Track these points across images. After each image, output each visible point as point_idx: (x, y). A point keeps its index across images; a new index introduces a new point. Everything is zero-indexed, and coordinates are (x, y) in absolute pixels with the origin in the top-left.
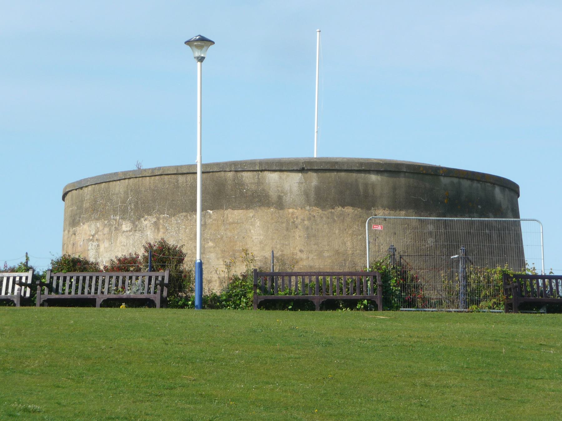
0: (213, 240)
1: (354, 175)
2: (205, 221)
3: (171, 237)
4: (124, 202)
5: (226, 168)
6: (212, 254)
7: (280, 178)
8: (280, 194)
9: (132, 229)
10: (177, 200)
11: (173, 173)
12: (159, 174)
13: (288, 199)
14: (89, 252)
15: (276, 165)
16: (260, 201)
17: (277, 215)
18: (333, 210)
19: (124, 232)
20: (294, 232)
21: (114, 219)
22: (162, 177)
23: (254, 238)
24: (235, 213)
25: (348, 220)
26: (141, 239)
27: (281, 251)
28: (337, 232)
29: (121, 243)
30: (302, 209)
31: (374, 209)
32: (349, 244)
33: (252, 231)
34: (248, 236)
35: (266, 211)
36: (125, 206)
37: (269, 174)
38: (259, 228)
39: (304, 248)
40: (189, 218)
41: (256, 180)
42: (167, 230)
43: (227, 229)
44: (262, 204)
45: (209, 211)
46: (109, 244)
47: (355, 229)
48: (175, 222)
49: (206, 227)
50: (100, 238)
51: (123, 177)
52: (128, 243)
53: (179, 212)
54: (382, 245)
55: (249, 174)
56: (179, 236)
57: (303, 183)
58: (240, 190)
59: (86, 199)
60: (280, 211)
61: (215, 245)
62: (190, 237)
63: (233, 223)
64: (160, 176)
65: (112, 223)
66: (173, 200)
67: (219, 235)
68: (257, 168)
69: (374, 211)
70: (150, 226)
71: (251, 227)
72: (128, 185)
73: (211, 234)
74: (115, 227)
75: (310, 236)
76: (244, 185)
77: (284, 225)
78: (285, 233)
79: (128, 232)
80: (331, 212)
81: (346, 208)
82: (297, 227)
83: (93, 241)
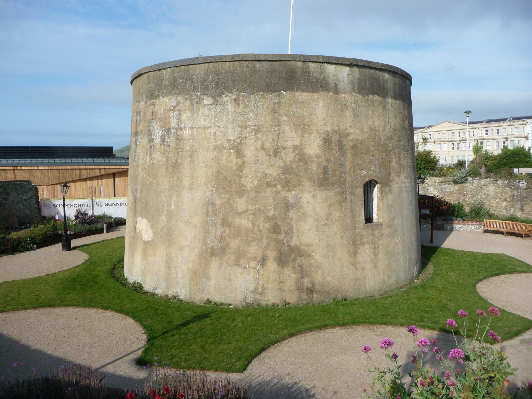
0: (287, 116)
1: (378, 72)
2: (280, 100)
3: (251, 111)
4: (204, 81)
6: (287, 127)
7: (336, 69)
9: (213, 103)
10: (255, 82)
11: (252, 59)
12: (238, 60)
13: (341, 86)
14: (171, 119)
15: (334, 59)
16: (322, 86)
17: (335, 98)
18: (368, 97)
19: (205, 105)
20: (346, 112)
21: (195, 95)
22: (241, 62)
23: (319, 115)
24: (304, 95)
27: (338, 126)
29: (203, 114)
30: (350, 94)
33: (317, 110)
34: (314, 113)
35: (327, 94)
36: (206, 85)
37: (328, 66)
40: (266, 96)
43: (298, 107)
44: (324, 89)
45: (283, 92)
48: (254, 99)
49: (280, 105)
50: (182, 109)
51: (204, 62)
52: (210, 114)
53: (257, 91)
55: (314, 64)
59: (165, 78)
60: (336, 95)
61: (288, 120)
64: (238, 62)
65: (193, 98)
66: (251, 82)
67: (292, 111)
68: (321, 60)
70: (231, 102)
71: (316, 107)
73: (285, 111)
74: (197, 101)
75: (356, 116)
77: (339, 106)
81: (375, 96)
83: (175, 111)
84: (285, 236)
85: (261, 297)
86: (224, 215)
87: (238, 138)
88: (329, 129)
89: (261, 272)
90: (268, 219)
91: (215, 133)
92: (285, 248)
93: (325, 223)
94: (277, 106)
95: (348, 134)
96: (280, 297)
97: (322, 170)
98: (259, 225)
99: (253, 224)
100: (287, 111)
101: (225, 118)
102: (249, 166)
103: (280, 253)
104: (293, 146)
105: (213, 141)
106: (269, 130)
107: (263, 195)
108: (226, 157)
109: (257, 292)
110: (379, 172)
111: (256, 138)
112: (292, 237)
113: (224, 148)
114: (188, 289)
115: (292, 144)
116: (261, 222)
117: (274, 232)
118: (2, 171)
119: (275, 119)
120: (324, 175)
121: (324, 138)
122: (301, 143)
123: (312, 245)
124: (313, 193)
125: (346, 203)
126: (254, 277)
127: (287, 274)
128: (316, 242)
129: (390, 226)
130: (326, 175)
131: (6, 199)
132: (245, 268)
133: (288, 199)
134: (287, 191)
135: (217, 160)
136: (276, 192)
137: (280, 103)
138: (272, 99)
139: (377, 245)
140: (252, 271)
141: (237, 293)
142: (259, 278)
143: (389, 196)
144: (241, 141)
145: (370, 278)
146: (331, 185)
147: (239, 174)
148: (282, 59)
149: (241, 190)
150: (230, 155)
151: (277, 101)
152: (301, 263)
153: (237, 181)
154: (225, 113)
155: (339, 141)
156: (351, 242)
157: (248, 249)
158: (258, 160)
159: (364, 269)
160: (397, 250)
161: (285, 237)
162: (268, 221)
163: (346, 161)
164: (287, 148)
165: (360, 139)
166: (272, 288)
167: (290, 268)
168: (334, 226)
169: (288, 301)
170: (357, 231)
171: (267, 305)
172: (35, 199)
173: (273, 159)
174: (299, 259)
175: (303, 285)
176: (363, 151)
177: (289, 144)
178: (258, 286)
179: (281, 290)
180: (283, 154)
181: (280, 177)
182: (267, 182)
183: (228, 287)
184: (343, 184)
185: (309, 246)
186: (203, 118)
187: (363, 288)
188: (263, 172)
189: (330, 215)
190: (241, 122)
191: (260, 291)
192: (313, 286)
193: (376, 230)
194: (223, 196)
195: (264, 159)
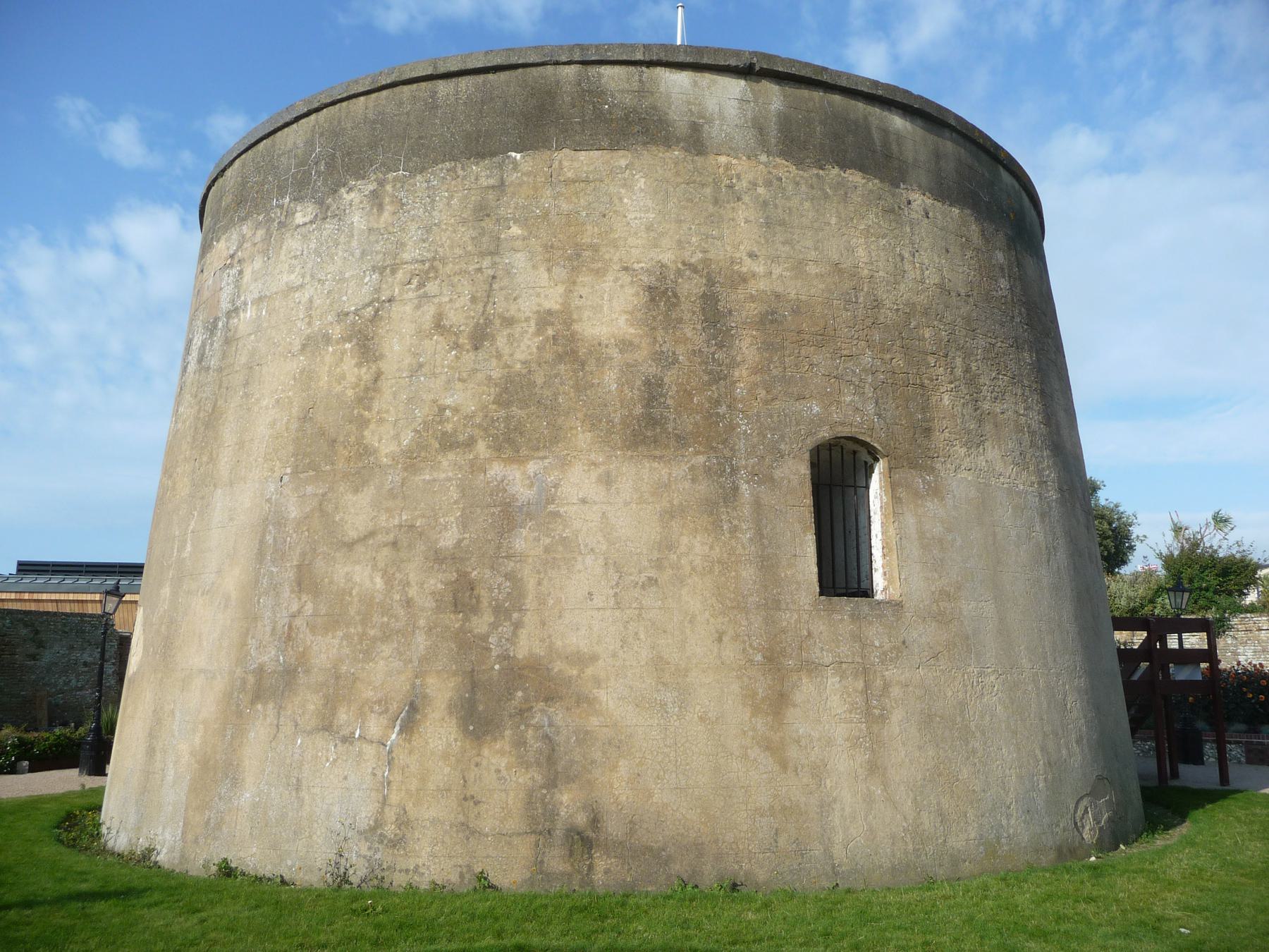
0: (523, 222)
4: (301, 164)
5: (559, 55)
6: (519, 255)
7: (695, 83)
8: (696, 120)
10: (432, 136)
13: (714, 132)
15: (685, 52)
16: (646, 132)
17: (691, 167)
18: (821, 172)
19: (298, 226)
21: (278, 206)
22: (397, 90)
23: (631, 216)
24: (582, 158)
25: (856, 198)
26: (336, 234)
27: (701, 251)
28: (833, 221)
30: (749, 158)
31: (905, 187)
32: (861, 252)
33: (625, 200)
34: (615, 212)
35: (661, 155)
36: (305, 172)
37: (667, 74)
38: (642, 194)
39: (760, 250)
40: (460, 172)
41: (636, 86)
42: (403, 204)
43: (560, 194)
45: (513, 154)
46: (264, 262)
47: (870, 223)
49: (503, 191)
53: (436, 162)
54: (927, 269)
55: (617, 70)
56: (433, 217)
57: (749, 101)
58: (593, 107)
60: (696, 158)
62: (460, 216)
63: (576, 181)
65: (273, 215)
66: (420, 138)
67: (537, 208)
69: (905, 191)
71: (623, 191)
72: (314, 126)
76: (606, 95)
77: (708, 191)
78: (711, 209)
79: (308, 226)
80: (817, 175)
81: (848, 171)
82: (739, 199)
84: (492, 620)
85: (393, 854)
86: (303, 554)
87: (368, 305)
88: (667, 257)
89: (401, 757)
90: (438, 558)
91: (311, 301)
92: (493, 668)
93: (650, 579)
94: (491, 196)
95: (744, 279)
96: (460, 862)
97: (639, 389)
98: (408, 583)
99: (389, 580)
100: (524, 207)
101: (340, 253)
102: (391, 387)
103: (473, 682)
104: (538, 312)
105: (301, 325)
106: (461, 269)
107: (427, 477)
108: (330, 367)
109: (381, 835)
110: (880, 416)
111: (420, 297)
112: (518, 626)
113: (327, 339)
114: (181, 824)
115: (535, 308)
116: (413, 571)
117: (456, 606)
118: (76, 604)
119: (482, 234)
120: (648, 405)
121: (650, 288)
122: (566, 306)
123: (594, 658)
124: (603, 468)
125: (735, 509)
126: (375, 775)
127: (493, 768)
128: (611, 648)
129: (941, 619)
130: (653, 407)
131: (34, 657)
132: (347, 740)
133: (512, 490)
134: (511, 460)
135: (306, 378)
136: (472, 466)
137: (501, 186)
138: (477, 179)
139: (879, 682)
140: (370, 750)
141: (315, 837)
142: (391, 778)
143: (929, 504)
144: (377, 311)
145: (848, 810)
146: (673, 442)
147: (362, 416)
148: (514, 60)
149: (360, 465)
150: (342, 360)
151: (492, 182)
152: (550, 725)
153: (352, 439)
154: (342, 239)
155: (704, 296)
156: (759, 657)
157: (363, 669)
158: (421, 366)
159: (819, 771)
160: (982, 717)
161: (494, 626)
162: (436, 566)
163: (734, 364)
164: (518, 321)
165: (792, 296)
166: (434, 822)
167: (504, 744)
168: (684, 591)
169: (496, 878)
170: (787, 618)
171: (412, 889)
172: (113, 664)
173: (468, 357)
174: (542, 711)
175: (552, 815)
176: (807, 337)
177: (527, 307)
178: (387, 810)
179: (468, 830)
180: (501, 341)
181: (486, 416)
182: (444, 434)
183: (290, 814)
184: (724, 442)
185: (582, 660)
186: (287, 266)
187: (817, 851)
188: (435, 401)
189: (670, 547)
190: (382, 255)
191: (390, 830)
192: (595, 821)
193: (871, 623)
194: (310, 489)
195: (439, 360)
